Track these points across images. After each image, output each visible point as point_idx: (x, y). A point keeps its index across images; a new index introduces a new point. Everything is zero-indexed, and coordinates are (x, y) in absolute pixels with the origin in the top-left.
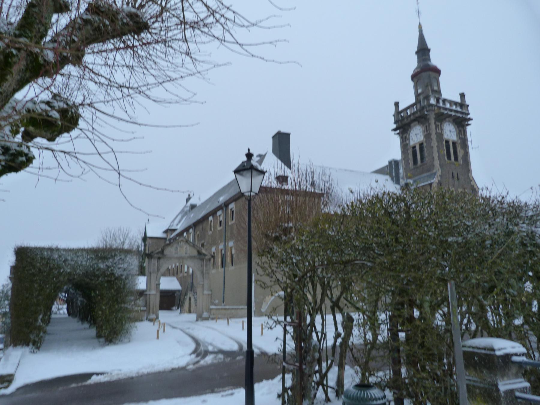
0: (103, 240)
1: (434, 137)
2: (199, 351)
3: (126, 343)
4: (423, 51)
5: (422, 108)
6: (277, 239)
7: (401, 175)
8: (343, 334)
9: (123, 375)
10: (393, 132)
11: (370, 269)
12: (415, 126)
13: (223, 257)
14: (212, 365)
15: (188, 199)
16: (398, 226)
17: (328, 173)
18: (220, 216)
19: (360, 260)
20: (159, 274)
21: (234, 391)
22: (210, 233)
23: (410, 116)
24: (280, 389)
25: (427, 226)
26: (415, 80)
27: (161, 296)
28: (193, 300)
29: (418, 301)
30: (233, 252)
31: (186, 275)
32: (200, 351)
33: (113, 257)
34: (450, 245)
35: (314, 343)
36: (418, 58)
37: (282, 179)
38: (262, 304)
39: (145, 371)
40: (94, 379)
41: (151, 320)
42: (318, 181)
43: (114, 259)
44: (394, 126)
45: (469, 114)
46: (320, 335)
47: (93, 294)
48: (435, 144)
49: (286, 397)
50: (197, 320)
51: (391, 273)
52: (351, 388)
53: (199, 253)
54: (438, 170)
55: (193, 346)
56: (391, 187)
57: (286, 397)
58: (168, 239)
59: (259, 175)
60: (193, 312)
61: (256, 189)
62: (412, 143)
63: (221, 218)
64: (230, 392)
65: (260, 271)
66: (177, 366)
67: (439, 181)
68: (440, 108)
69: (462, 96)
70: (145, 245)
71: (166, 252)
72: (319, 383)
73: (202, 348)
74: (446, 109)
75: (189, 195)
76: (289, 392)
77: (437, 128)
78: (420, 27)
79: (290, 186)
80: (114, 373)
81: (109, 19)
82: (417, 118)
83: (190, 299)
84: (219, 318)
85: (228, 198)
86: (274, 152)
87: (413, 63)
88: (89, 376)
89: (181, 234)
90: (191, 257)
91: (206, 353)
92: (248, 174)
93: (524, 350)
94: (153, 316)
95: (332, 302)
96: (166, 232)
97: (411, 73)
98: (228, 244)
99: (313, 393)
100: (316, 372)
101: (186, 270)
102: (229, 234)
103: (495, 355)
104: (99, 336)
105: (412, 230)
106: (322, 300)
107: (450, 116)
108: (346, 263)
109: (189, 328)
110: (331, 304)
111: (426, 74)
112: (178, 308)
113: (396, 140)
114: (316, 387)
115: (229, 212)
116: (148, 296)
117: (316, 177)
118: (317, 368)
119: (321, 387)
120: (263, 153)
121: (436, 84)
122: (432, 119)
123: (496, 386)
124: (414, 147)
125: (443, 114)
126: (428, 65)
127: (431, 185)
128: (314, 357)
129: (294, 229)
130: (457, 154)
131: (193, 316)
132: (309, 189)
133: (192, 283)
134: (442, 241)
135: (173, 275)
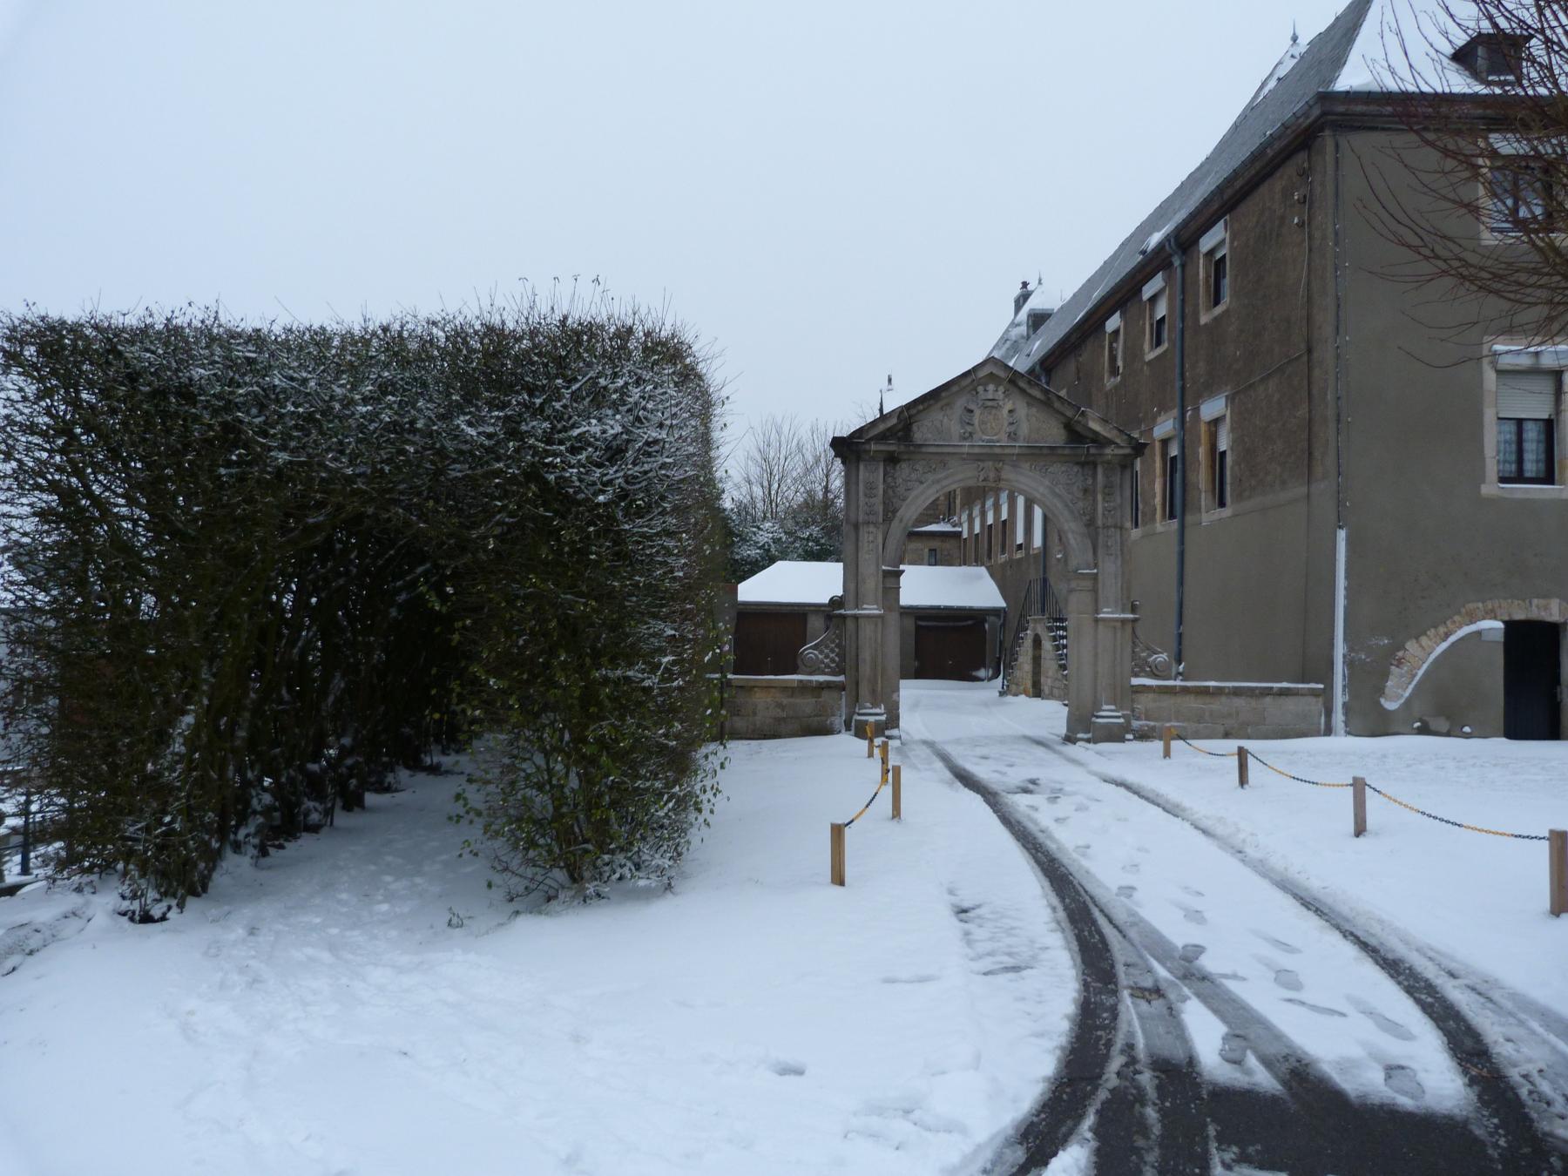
3: (647, 895)
18: (1154, 299)
22: (1110, 382)
28: (1047, 645)
30: (1223, 444)
31: (1019, 555)
38: (1385, 676)
41: (860, 732)
50: (1070, 739)
53: (1076, 434)
60: (1051, 696)
63: (1161, 310)
71: (921, 433)
75: (1025, 285)
83: (1037, 642)
90: (1038, 454)
98: (1197, 410)
101: (1020, 539)
102: (1202, 367)
112: (996, 676)
116: (850, 624)
131: (1051, 715)
133: (1045, 580)
135: (978, 562)
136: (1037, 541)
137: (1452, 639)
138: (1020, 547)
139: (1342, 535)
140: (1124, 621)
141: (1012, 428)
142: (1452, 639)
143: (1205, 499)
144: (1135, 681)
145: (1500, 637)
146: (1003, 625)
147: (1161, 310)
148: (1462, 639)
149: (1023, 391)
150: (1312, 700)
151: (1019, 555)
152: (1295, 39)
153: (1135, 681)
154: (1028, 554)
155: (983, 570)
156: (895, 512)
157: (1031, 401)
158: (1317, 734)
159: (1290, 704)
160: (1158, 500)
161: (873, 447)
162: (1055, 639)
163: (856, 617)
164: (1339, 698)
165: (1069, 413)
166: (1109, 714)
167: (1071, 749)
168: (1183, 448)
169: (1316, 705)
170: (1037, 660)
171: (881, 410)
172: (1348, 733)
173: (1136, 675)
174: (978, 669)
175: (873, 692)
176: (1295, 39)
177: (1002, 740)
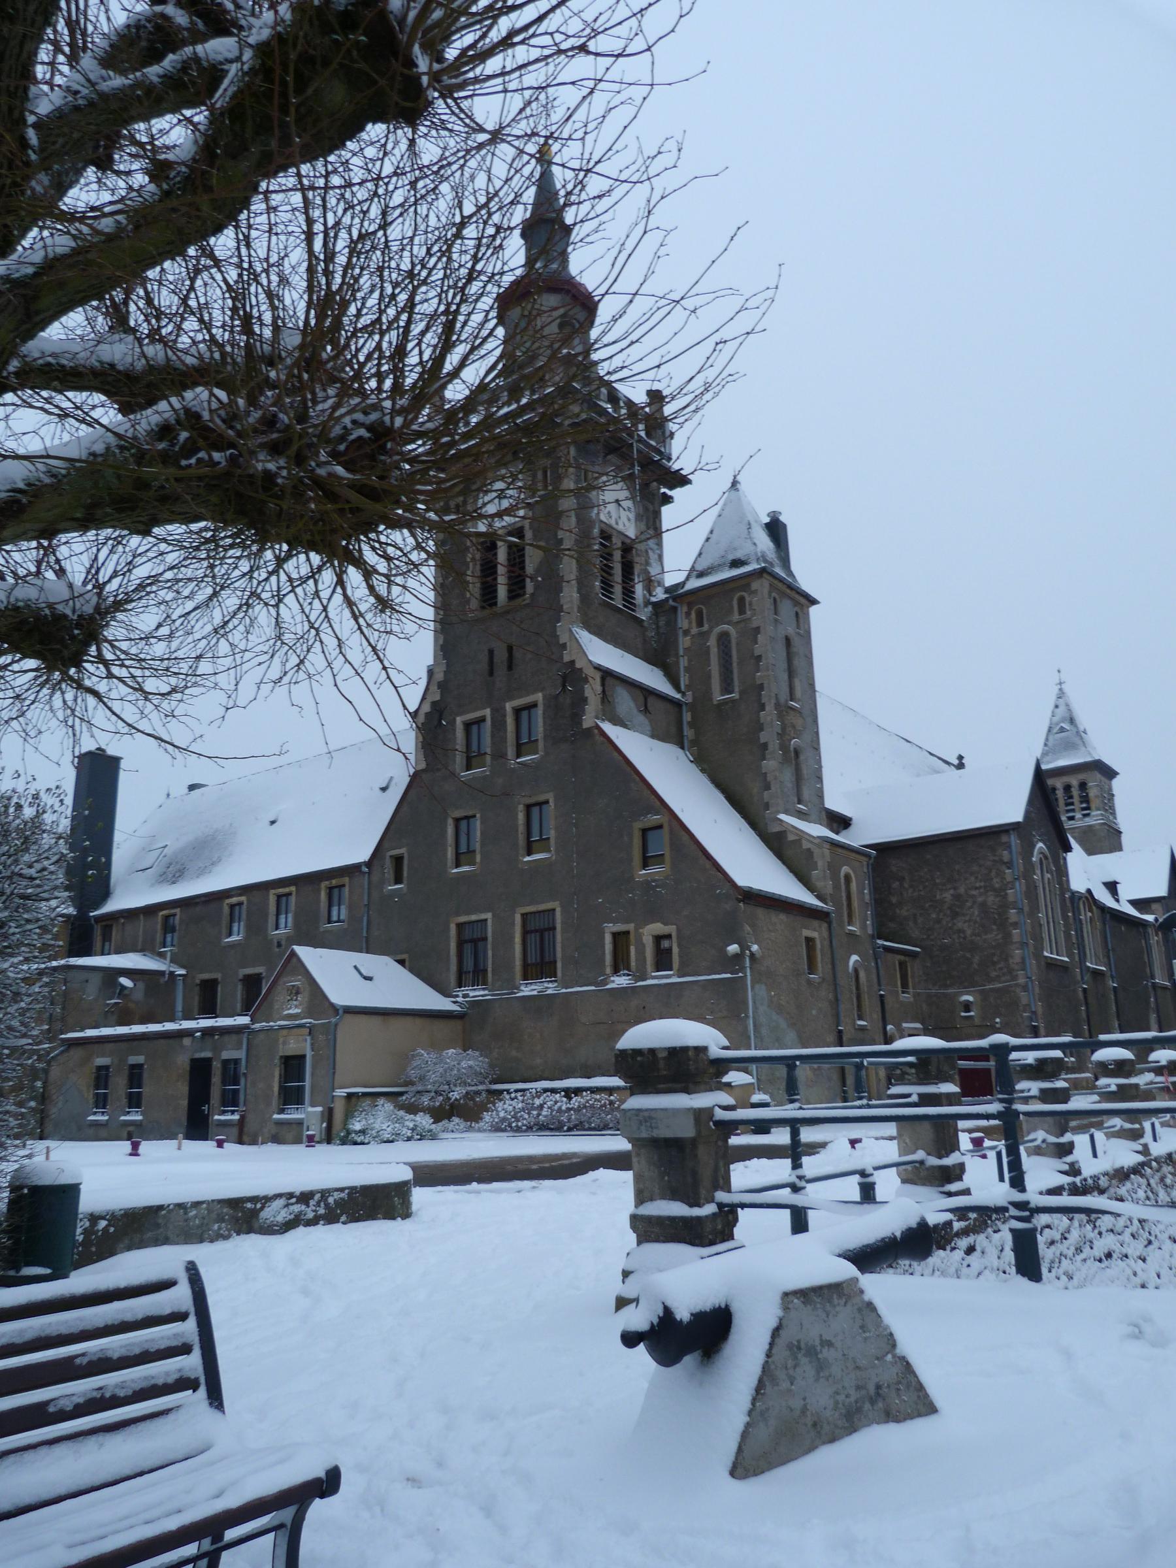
124: (489, 543)
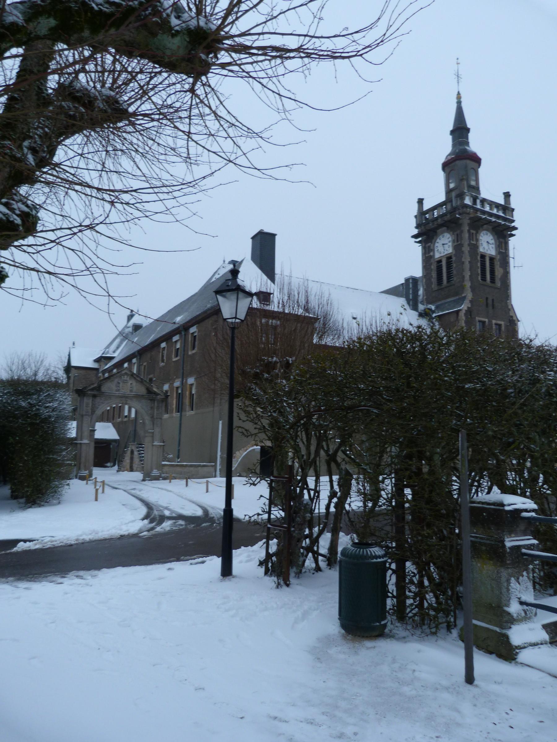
0: (8, 369)
1: (466, 249)
2: (152, 516)
3: (54, 505)
4: (460, 131)
5: (454, 210)
6: (257, 376)
7: (420, 298)
8: (339, 494)
9: (58, 542)
10: (414, 240)
11: (377, 417)
12: (442, 233)
13: (180, 397)
14: (171, 532)
15: (130, 317)
16: (411, 369)
17: (326, 295)
18: (176, 342)
19: (364, 406)
20: (94, 417)
21: (204, 559)
22: (162, 364)
23: (437, 219)
24: (262, 555)
25: (443, 370)
26: (448, 169)
27: (96, 448)
28: (136, 453)
29: (428, 454)
30: (193, 392)
31: (126, 420)
32: (153, 515)
33: (38, 392)
34: (467, 392)
35: (305, 502)
36: (454, 140)
37: (265, 297)
39: (87, 538)
40: (21, 546)
41: (82, 478)
42: (314, 303)
43: (39, 396)
44: (416, 231)
45: (513, 221)
46: (312, 493)
47: (11, 440)
48: (467, 259)
49: (270, 565)
50: (144, 480)
51: (400, 422)
52: (349, 546)
53: (149, 391)
54: (469, 295)
55: (144, 511)
56: (408, 319)
57: (270, 565)
58: (101, 370)
59: (247, 297)
60: (137, 471)
61: (242, 315)
62: (437, 256)
63: (178, 346)
64: (201, 560)
65: (243, 416)
66: (126, 533)
67: (468, 307)
68: (477, 210)
69: (507, 195)
70: (69, 378)
71: (104, 389)
72: (309, 549)
73: (156, 513)
74: (484, 212)
76: (274, 559)
77: (471, 236)
78: (459, 93)
79: (274, 307)
80: (47, 539)
81: (84, 105)
82: (446, 222)
83: (132, 452)
84: (175, 478)
85: (189, 318)
86: (254, 259)
87: (445, 147)
88: (15, 542)
89: (119, 364)
90: (138, 397)
91: (162, 519)
92: (233, 296)
93: (535, 506)
94: (85, 473)
95: (328, 455)
96: (97, 361)
97: (443, 160)
98: (186, 380)
99: (301, 559)
100: (306, 537)
101: (126, 413)
103: (504, 510)
104: (14, 496)
105: (427, 374)
106: (317, 453)
107: (490, 222)
108: (350, 408)
109: (134, 489)
110: (327, 458)
111: (462, 163)
112: (114, 465)
113: (417, 250)
114: (305, 553)
115: (190, 338)
116: (79, 446)
117: (312, 298)
118: (307, 532)
119: (310, 555)
120: (239, 260)
121: (474, 178)
122: (465, 231)
123: (503, 542)
124: (440, 261)
125: (480, 219)
126: (466, 151)
127: (458, 312)
128: (304, 518)
129: (279, 365)
130: (494, 277)
132: (301, 312)
133: (135, 431)
134: (458, 387)
135: (108, 421)
136: (133, 415)
137: (248, 451)
138: (126, 416)
139: (221, 422)
140: (161, 445)
141: (131, 389)
142: (248, 451)
143: (188, 408)
144: (163, 463)
145: (259, 450)
146: (118, 446)
147: (178, 346)
148: (250, 451)
149: (135, 378)
150: (211, 468)
151: (126, 420)
152: (224, 261)
153: (163, 463)
154: (129, 419)
155: (110, 424)
156: (94, 412)
157: (137, 381)
158: (212, 477)
159: (205, 469)
160: (174, 406)
161: (89, 392)
162: (139, 451)
163: (81, 444)
164: (218, 467)
165: (148, 385)
166: (155, 472)
167: (144, 483)
168: (182, 391)
169: (212, 469)
170: (132, 459)
171: (187, 482)
172: (221, 477)
173: (164, 461)
174: (107, 463)
175: (85, 466)
176: (224, 261)
177: (124, 481)
